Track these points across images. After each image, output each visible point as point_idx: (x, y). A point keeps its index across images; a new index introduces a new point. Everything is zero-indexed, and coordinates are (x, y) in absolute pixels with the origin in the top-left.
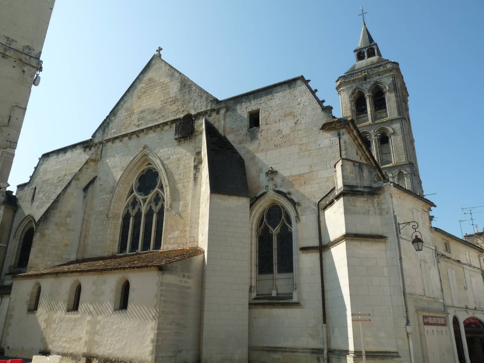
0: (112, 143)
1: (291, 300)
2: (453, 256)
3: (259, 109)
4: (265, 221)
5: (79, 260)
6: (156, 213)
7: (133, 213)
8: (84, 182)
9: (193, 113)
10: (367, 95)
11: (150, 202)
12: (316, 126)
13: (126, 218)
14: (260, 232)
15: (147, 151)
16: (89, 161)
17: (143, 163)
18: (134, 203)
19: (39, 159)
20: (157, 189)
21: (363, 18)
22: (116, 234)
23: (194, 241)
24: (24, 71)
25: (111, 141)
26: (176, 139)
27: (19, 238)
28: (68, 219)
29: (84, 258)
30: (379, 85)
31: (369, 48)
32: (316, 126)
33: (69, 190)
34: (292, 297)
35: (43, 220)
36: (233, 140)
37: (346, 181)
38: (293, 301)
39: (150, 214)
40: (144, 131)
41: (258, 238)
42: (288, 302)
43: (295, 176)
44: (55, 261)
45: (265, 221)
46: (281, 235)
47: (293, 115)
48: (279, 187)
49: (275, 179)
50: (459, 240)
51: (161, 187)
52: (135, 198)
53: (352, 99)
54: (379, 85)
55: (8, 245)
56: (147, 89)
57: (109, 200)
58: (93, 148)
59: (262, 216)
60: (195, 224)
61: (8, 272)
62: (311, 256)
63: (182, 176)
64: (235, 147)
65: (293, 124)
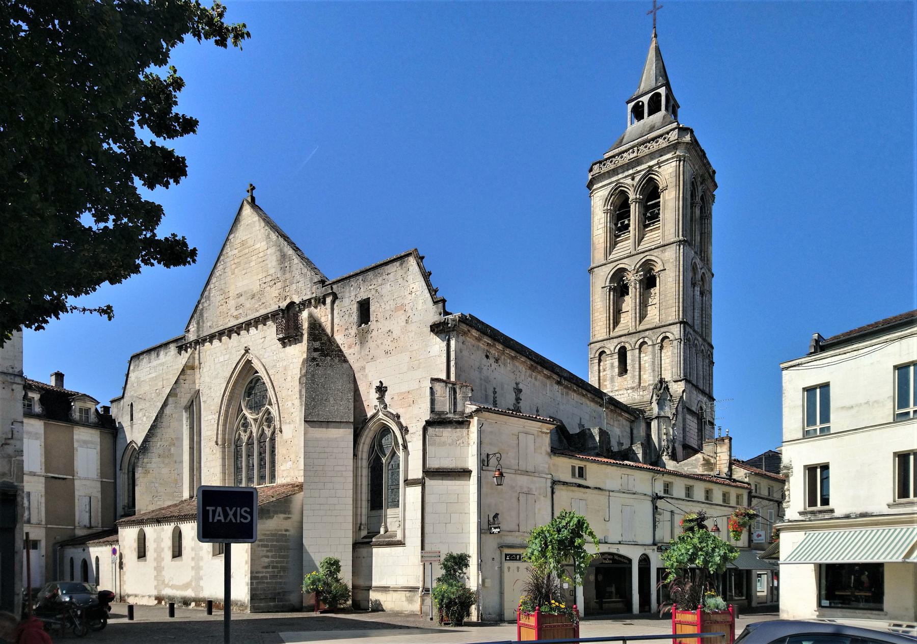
2: (589, 482)
8: (184, 400)
9: (297, 300)
10: (632, 196)
14: (372, 461)
15: (249, 357)
16: (185, 369)
20: (267, 406)
21: (655, 20)
24: (13, 390)
26: (279, 340)
27: (126, 472)
30: (653, 176)
31: (650, 95)
33: (168, 411)
36: (342, 342)
39: (261, 440)
51: (270, 404)
53: (609, 207)
54: (653, 176)
56: (241, 258)
58: (189, 350)
59: (373, 445)
61: (123, 513)
63: (290, 390)
65: (404, 323)
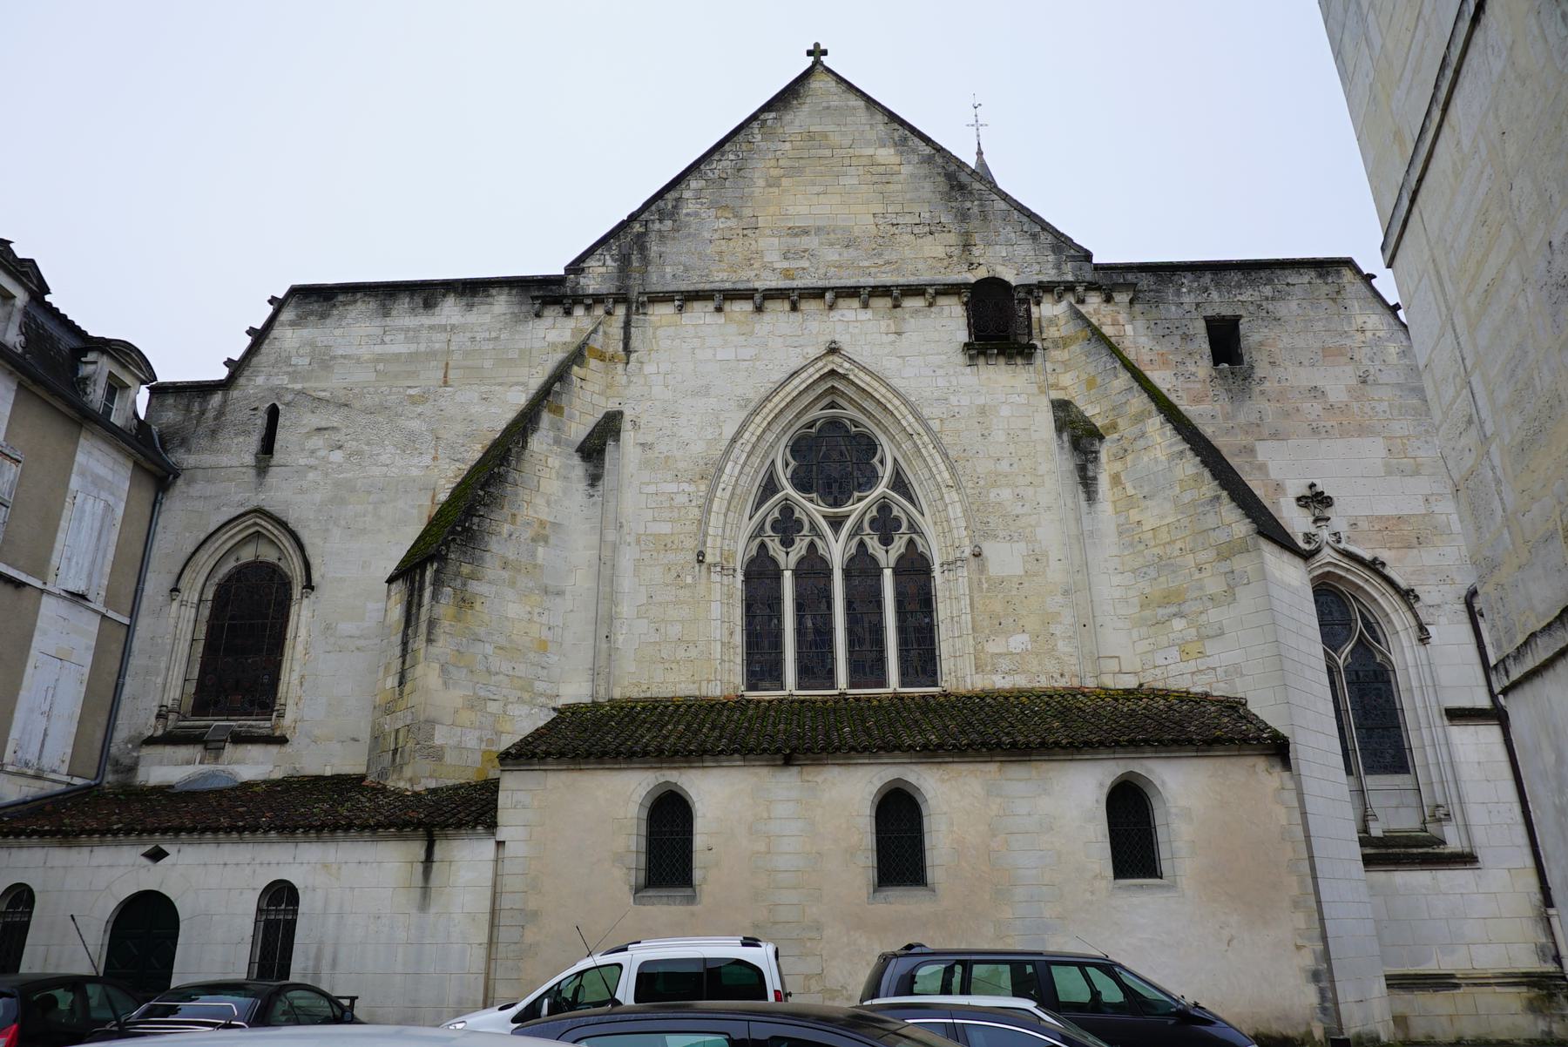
0: (680, 309)
1: (1442, 847)
3: (1240, 317)
6: (793, 570)
7: (788, 559)
11: (857, 529)
13: (760, 573)
17: (818, 398)
18: (787, 526)
19: (271, 302)
20: (881, 489)
23: (1504, 663)
25: (677, 303)
28: (541, 551)
35: (458, 541)
37: (864, 549)
40: (827, 294)
43: (1388, 518)
44: (512, 703)
46: (1357, 673)
47: (1349, 355)
52: (787, 509)
55: (134, 613)
57: (694, 504)
58: (579, 311)
60: (1115, 618)
62: (1477, 732)
64: (1182, 408)
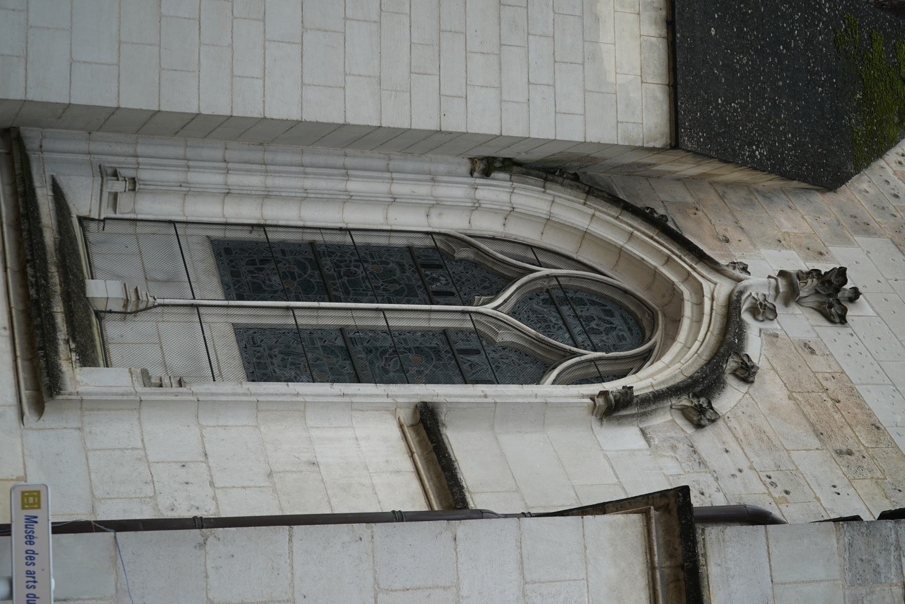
1: (74, 357)
4: (535, 271)
5: (434, 448)
12: (869, 180)
22: (593, 215)
29: (442, 417)
32: (869, 180)
34: (94, 364)
38: (65, 366)
41: (428, 242)
42: (61, 342)
43: (861, 405)
45: (583, 358)
48: (768, 326)
49: (795, 309)
50: (442, 517)
